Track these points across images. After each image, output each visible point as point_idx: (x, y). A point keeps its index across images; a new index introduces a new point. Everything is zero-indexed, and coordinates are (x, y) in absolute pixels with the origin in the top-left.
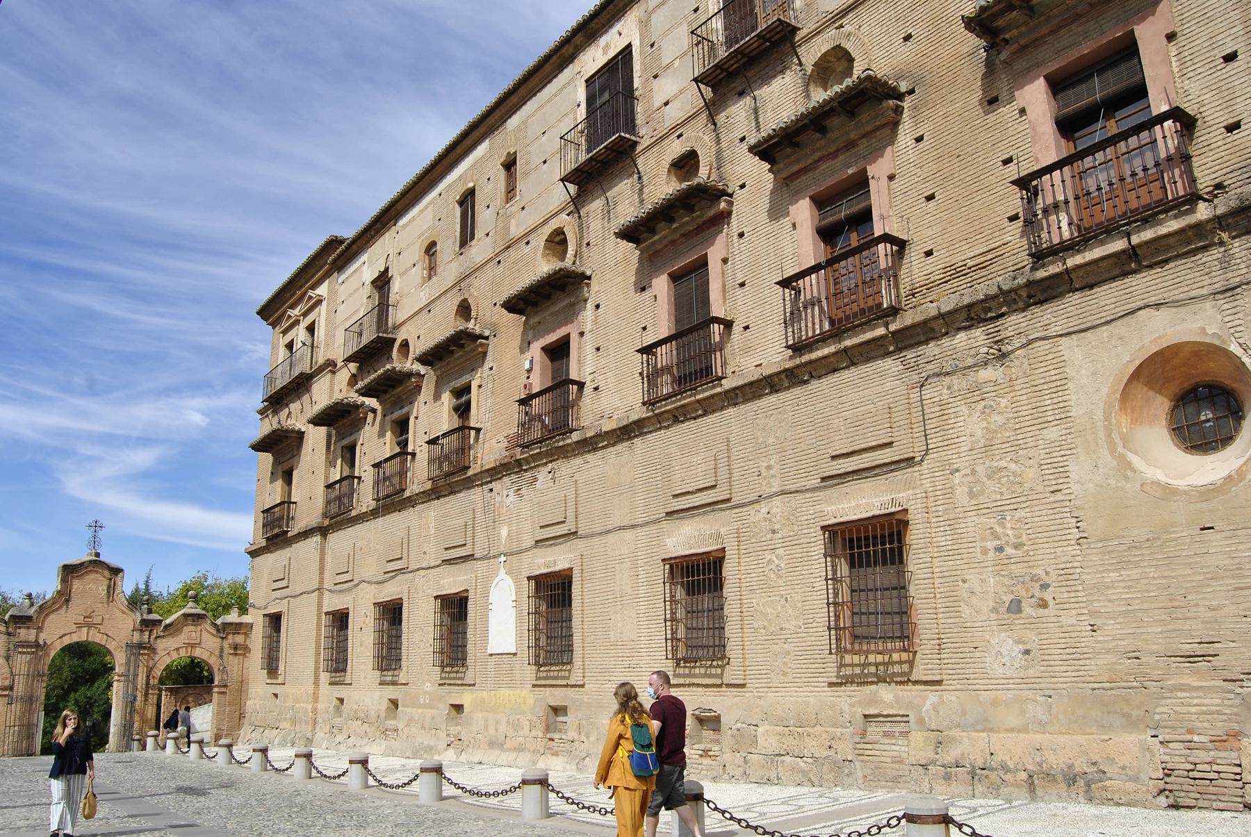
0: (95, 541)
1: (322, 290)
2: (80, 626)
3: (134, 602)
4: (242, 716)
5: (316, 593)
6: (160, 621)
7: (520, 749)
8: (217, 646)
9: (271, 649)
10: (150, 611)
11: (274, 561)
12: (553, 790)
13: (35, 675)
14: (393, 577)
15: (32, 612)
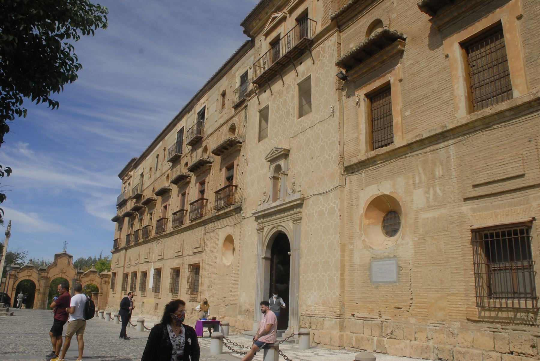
1: (132, 173)
2: (59, 273)
3: (76, 266)
4: (107, 303)
7: (151, 314)
9: (156, 283)
10: (80, 269)
11: (116, 255)
12: (281, 354)
13: (46, 287)
15: (46, 268)
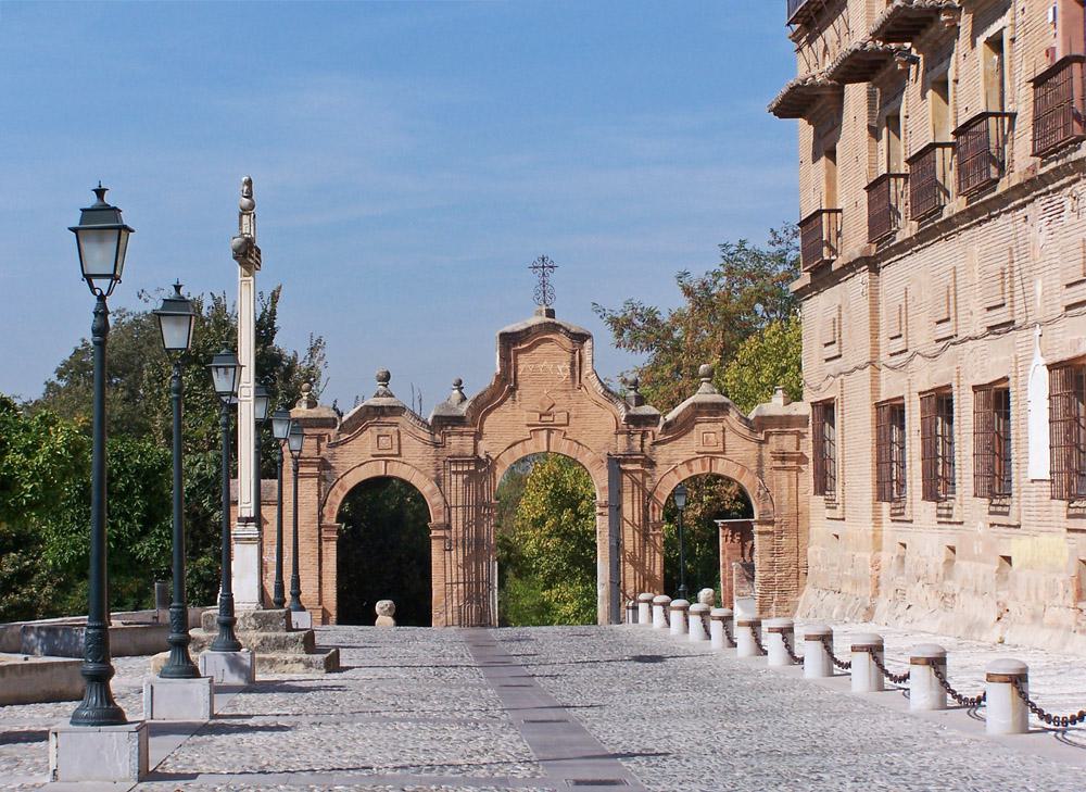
0: (544, 289)
2: (535, 429)
5: (868, 370)
6: (655, 418)
8: (753, 454)
14: (319, 495)
15: (463, 410)
